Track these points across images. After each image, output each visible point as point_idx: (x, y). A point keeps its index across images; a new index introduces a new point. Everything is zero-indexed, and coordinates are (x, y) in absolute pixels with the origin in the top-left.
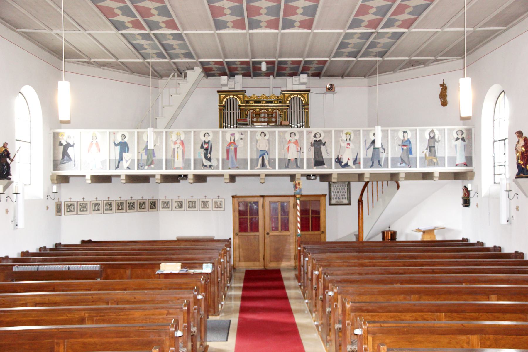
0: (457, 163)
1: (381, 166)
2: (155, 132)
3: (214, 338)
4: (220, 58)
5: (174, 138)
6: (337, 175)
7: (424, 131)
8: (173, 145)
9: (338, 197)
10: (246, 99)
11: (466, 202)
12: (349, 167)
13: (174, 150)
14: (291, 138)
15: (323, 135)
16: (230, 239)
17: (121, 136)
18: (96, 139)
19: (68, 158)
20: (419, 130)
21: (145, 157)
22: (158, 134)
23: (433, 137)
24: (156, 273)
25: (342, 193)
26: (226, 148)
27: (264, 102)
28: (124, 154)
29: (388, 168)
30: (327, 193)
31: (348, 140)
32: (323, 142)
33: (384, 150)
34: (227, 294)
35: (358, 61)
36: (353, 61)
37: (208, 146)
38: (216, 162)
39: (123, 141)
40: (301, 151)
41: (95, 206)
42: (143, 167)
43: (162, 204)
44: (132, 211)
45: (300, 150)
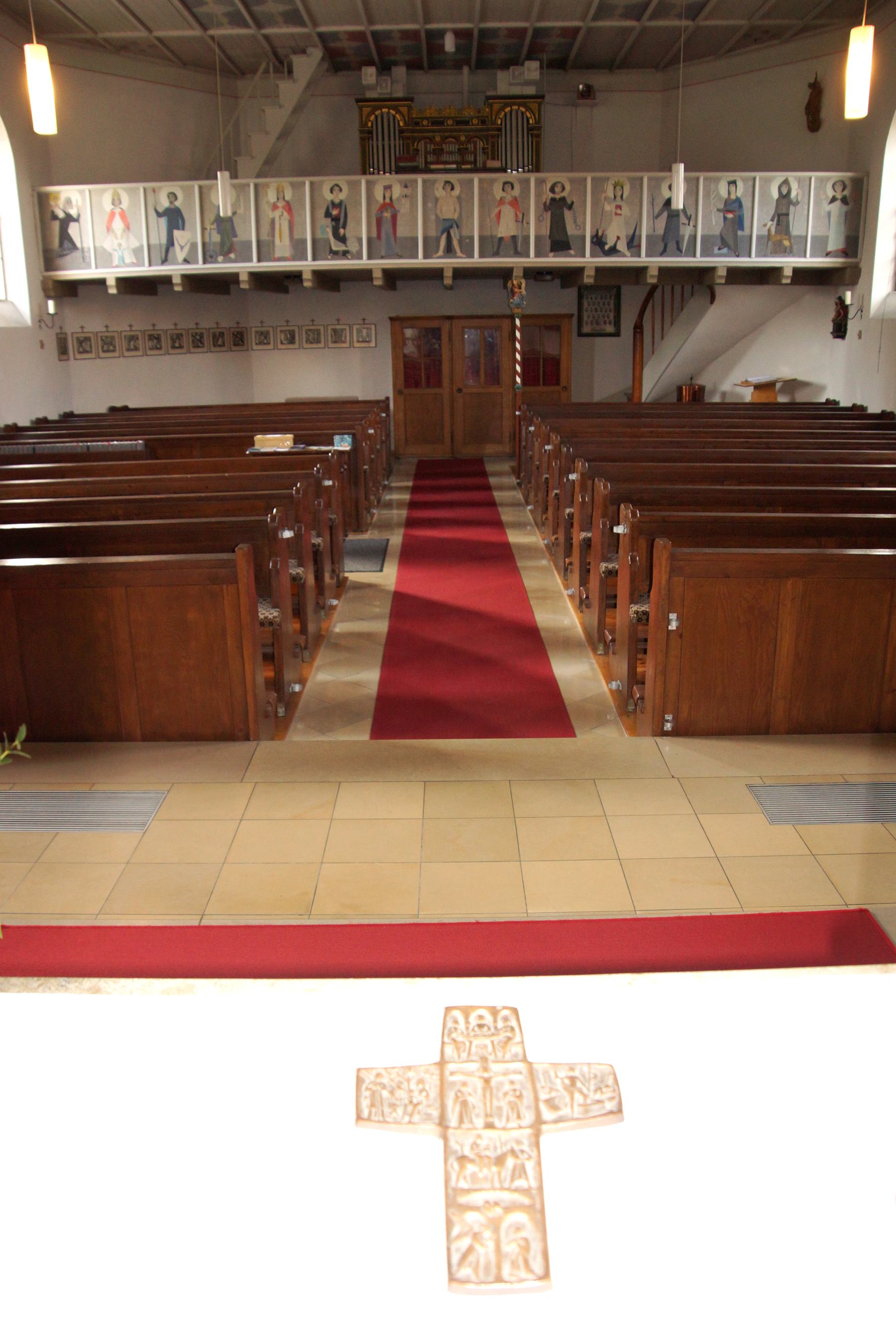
0: (829, 249)
1: (681, 252)
2: (234, 186)
3: (358, 567)
4: (358, 23)
5: (272, 196)
6: (594, 270)
7: (768, 181)
8: (270, 211)
9: (596, 320)
10: (414, 116)
11: (840, 331)
12: (619, 253)
13: (273, 222)
14: (504, 194)
15: (568, 187)
16: (388, 399)
17: (168, 197)
18: (120, 203)
19: (70, 245)
20: (760, 178)
21: (216, 238)
22: (241, 190)
23: (786, 195)
24: (247, 452)
25: (604, 312)
26: (376, 215)
27: (450, 122)
28: (177, 233)
29: (694, 256)
30: (574, 311)
31: (618, 198)
32: (569, 202)
33: (689, 219)
34: (383, 498)
35: (644, 30)
36: (632, 29)
37: (340, 212)
38: (357, 244)
39: (172, 207)
40: (524, 221)
41: (130, 342)
42: (214, 257)
43: (256, 336)
44: (199, 350)
45: (522, 219)
